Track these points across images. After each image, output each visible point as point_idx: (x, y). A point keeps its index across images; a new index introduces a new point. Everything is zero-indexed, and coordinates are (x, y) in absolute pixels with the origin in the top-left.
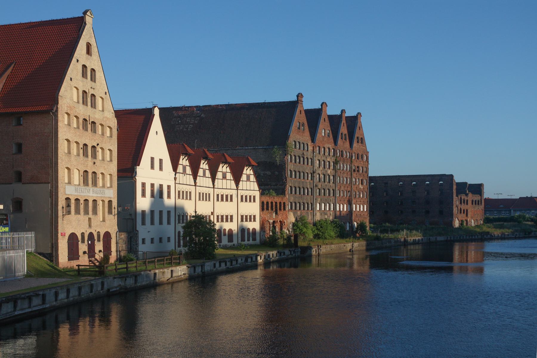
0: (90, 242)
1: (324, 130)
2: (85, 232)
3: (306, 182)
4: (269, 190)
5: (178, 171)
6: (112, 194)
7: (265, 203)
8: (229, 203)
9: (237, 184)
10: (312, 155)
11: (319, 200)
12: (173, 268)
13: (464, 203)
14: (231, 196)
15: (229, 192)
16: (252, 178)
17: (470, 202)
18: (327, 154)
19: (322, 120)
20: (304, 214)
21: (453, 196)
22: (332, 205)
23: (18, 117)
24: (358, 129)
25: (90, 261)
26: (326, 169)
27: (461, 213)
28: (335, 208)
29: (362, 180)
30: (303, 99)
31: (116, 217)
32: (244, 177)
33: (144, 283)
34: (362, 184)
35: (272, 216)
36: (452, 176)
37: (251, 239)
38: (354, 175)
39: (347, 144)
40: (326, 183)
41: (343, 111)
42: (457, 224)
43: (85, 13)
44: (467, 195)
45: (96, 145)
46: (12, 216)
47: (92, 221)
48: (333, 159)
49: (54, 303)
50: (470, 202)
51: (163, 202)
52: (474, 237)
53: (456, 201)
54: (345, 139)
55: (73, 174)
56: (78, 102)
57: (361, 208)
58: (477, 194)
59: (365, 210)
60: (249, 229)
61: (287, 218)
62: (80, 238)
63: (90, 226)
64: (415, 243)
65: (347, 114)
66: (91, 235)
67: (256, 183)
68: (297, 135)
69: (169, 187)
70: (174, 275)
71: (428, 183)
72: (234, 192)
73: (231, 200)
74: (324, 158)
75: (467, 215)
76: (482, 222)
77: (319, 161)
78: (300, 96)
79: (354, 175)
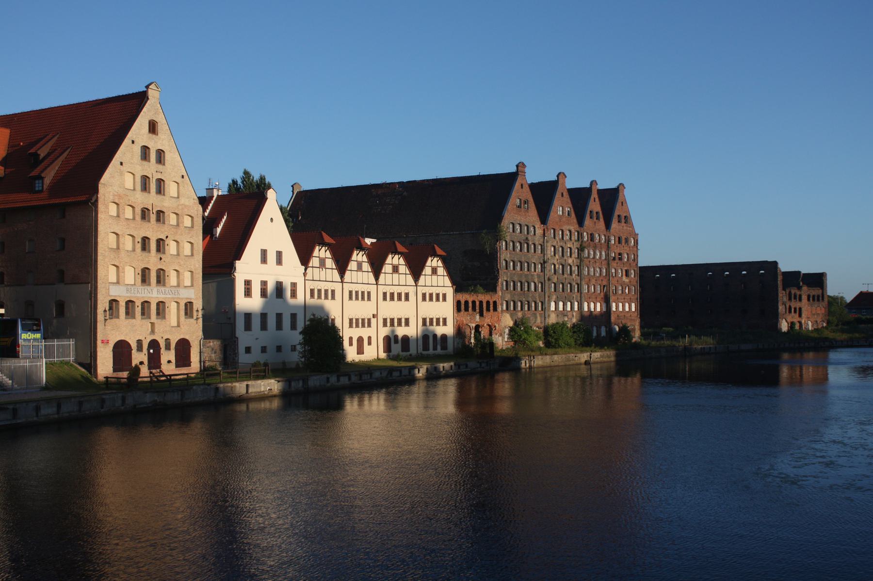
0: (151, 351)
1: (561, 208)
2: (143, 339)
3: (532, 275)
4: (475, 286)
5: (310, 265)
6: (194, 294)
7: (463, 303)
8: (366, 302)
9: (377, 277)
10: (542, 240)
11: (554, 297)
12: (249, 383)
13: (795, 298)
14: (369, 293)
15: (366, 288)
16: (441, 271)
17: (804, 298)
18: (567, 238)
19: (558, 195)
20: (528, 315)
21: (777, 290)
22: (576, 304)
23: (63, 209)
24: (618, 206)
25: (151, 373)
26: (565, 258)
27: (790, 312)
28: (580, 307)
29: (627, 271)
30: (526, 170)
31: (200, 321)
32: (353, 265)
33: (197, 399)
34: (627, 275)
35: (475, 317)
36: (775, 263)
37: (439, 347)
38: (614, 264)
39: (601, 224)
40: (566, 276)
41: (593, 183)
42: (784, 326)
43: (147, 87)
44: (799, 288)
45: (164, 238)
46: (55, 321)
47: (156, 326)
48: (577, 245)
49: (35, 419)
50: (804, 298)
51: (285, 301)
52: (806, 344)
53: (782, 296)
54: (598, 218)
55: (124, 272)
56: (134, 189)
57: (626, 308)
58: (816, 287)
59: (633, 309)
60: (435, 336)
61: (499, 320)
62: (134, 345)
63: (153, 332)
64: (703, 352)
65: (601, 186)
66: (154, 344)
67: (447, 278)
68: (518, 216)
69: (294, 285)
70: (250, 391)
71: (744, 272)
72: (411, 290)
73: (369, 299)
74: (562, 244)
75: (800, 316)
76: (825, 325)
77: (554, 247)
78: (521, 166)
79: (614, 264)
